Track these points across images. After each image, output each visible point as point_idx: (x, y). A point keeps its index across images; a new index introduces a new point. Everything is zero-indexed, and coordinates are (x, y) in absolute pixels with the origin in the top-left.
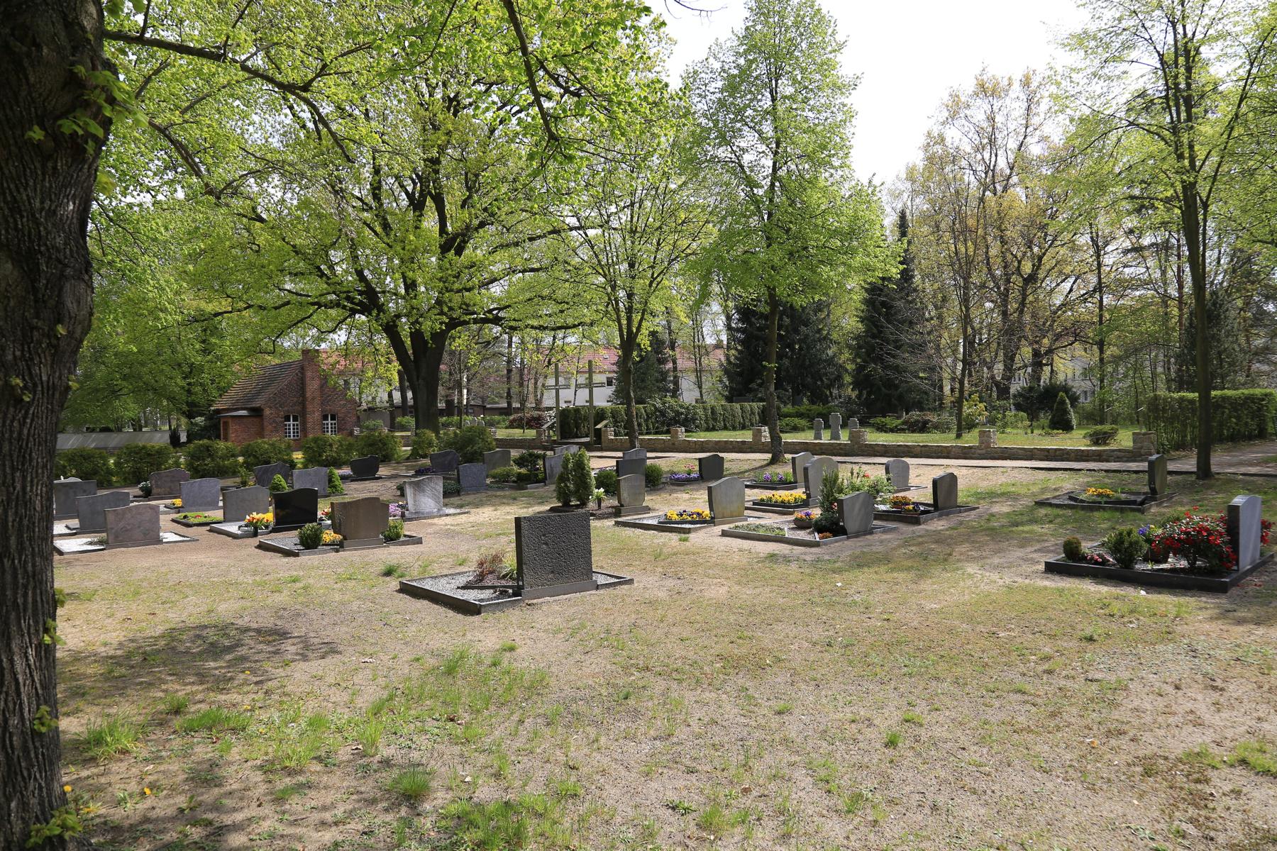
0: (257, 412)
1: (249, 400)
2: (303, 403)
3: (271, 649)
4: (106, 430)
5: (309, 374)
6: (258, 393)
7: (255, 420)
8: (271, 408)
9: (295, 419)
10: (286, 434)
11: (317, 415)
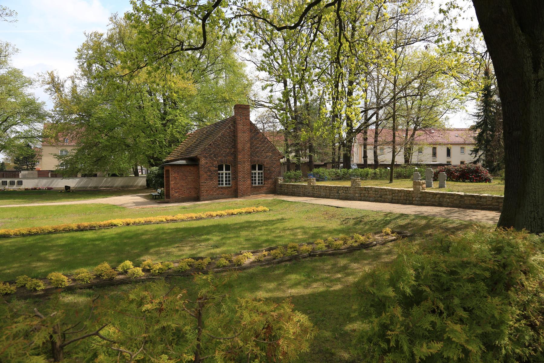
0: (194, 162)
1: (190, 152)
2: (235, 154)
3: (479, 202)
4: (114, 175)
5: (240, 127)
6: (196, 146)
7: (192, 168)
8: (206, 157)
9: (228, 169)
10: (220, 181)
11: (248, 166)
